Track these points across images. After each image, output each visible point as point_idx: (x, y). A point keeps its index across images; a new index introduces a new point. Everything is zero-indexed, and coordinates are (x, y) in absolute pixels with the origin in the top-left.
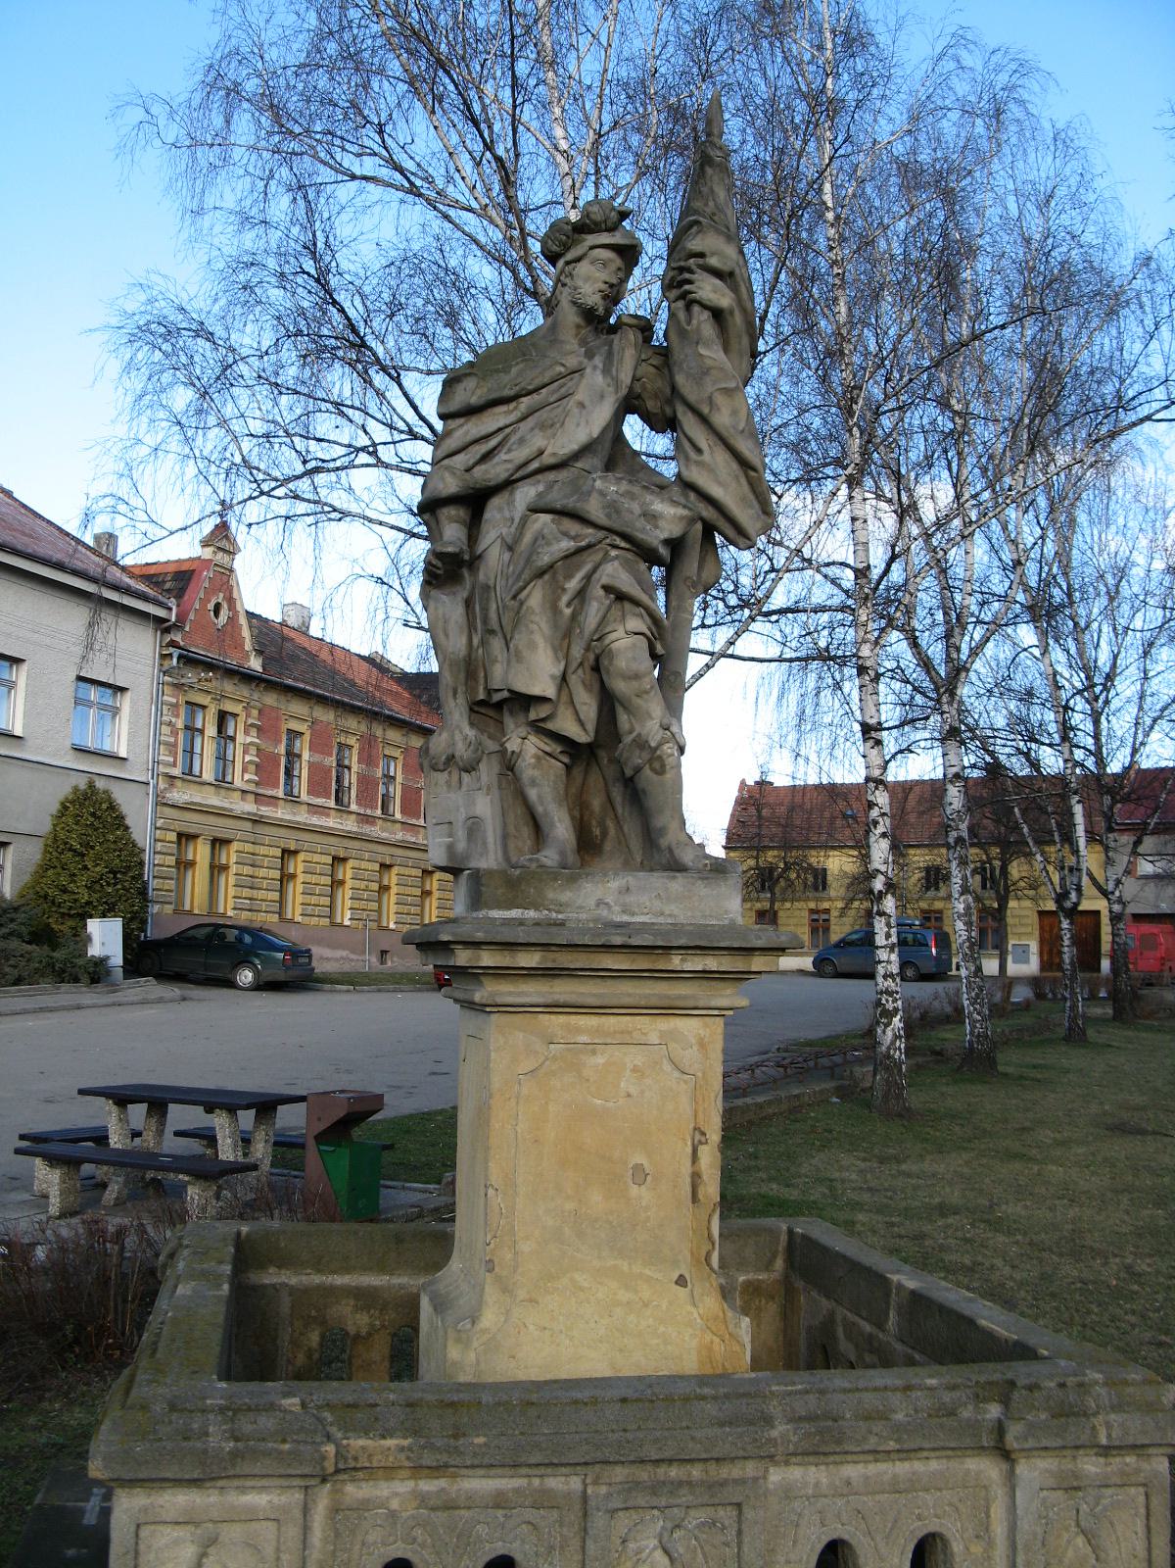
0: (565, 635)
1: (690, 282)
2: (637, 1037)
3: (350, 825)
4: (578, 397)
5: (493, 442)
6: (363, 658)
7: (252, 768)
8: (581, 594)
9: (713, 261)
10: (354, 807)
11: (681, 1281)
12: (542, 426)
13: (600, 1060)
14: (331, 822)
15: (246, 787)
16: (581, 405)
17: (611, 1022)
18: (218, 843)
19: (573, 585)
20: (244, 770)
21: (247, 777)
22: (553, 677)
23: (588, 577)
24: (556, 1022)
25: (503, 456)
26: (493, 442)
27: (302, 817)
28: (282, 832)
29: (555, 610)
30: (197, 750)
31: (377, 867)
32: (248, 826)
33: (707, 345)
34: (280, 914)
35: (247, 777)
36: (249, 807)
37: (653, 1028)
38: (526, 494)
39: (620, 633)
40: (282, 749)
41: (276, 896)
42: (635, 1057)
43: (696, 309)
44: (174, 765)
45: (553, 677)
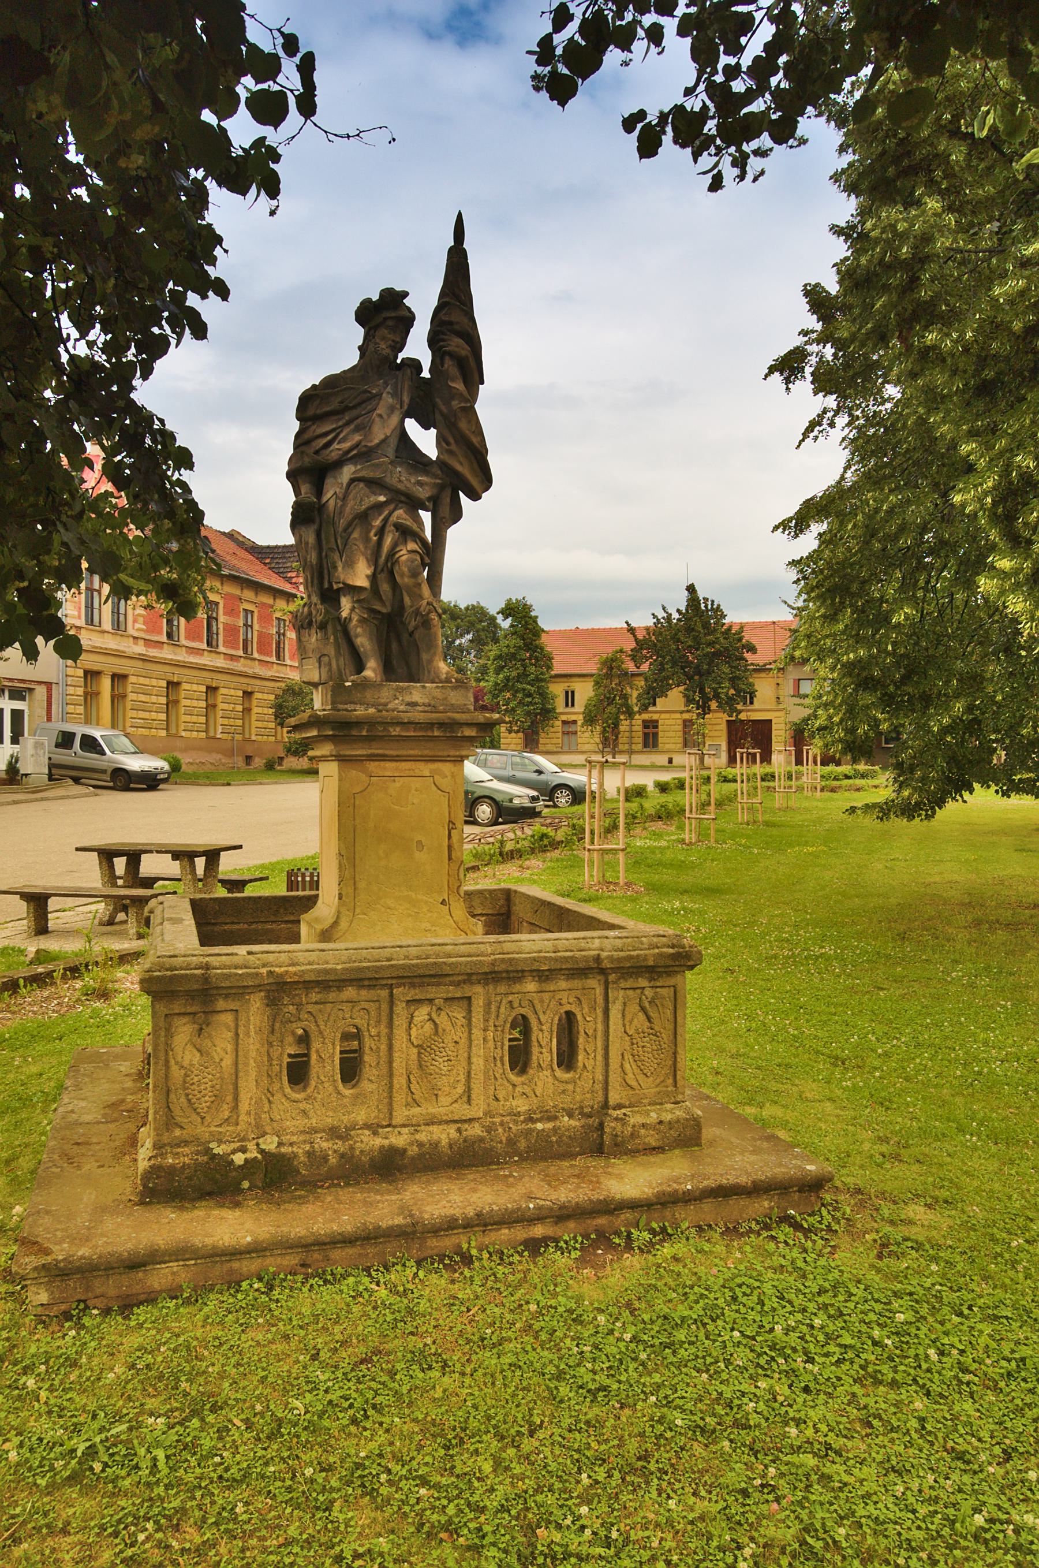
0: (374, 559)
1: (443, 340)
2: (417, 773)
3: (220, 662)
4: (378, 412)
5: (329, 437)
6: (224, 534)
7: (141, 620)
8: (381, 532)
9: (457, 327)
10: (221, 649)
11: (443, 903)
12: (357, 429)
13: (397, 785)
14: (206, 660)
15: (136, 634)
16: (380, 416)
17: (404, 765)
18: (119, 678)
19: (377, 523)
20: (135, 621)
21: (137, 626)
22: (367, 576)
23: (386, 520)
24: (372, 766)
25: (335, 446)
26: (329, 437)
27: (182, 656)
28: (167, 668)
29: (367, 540)
30: (122, 611)
31: (240, 693)
32: (140, 664)
33: (453, 380)
34: (167, 729)
35: (137, 626)
36: (140, 649)
37: (425, 769)
38: (348, 472)
39: (404, 552)
40: (241, 623)
41: (163, 716)
42: (416, 783)
43: (447, 358)
44: (79, 618)
45: (367, 576)
